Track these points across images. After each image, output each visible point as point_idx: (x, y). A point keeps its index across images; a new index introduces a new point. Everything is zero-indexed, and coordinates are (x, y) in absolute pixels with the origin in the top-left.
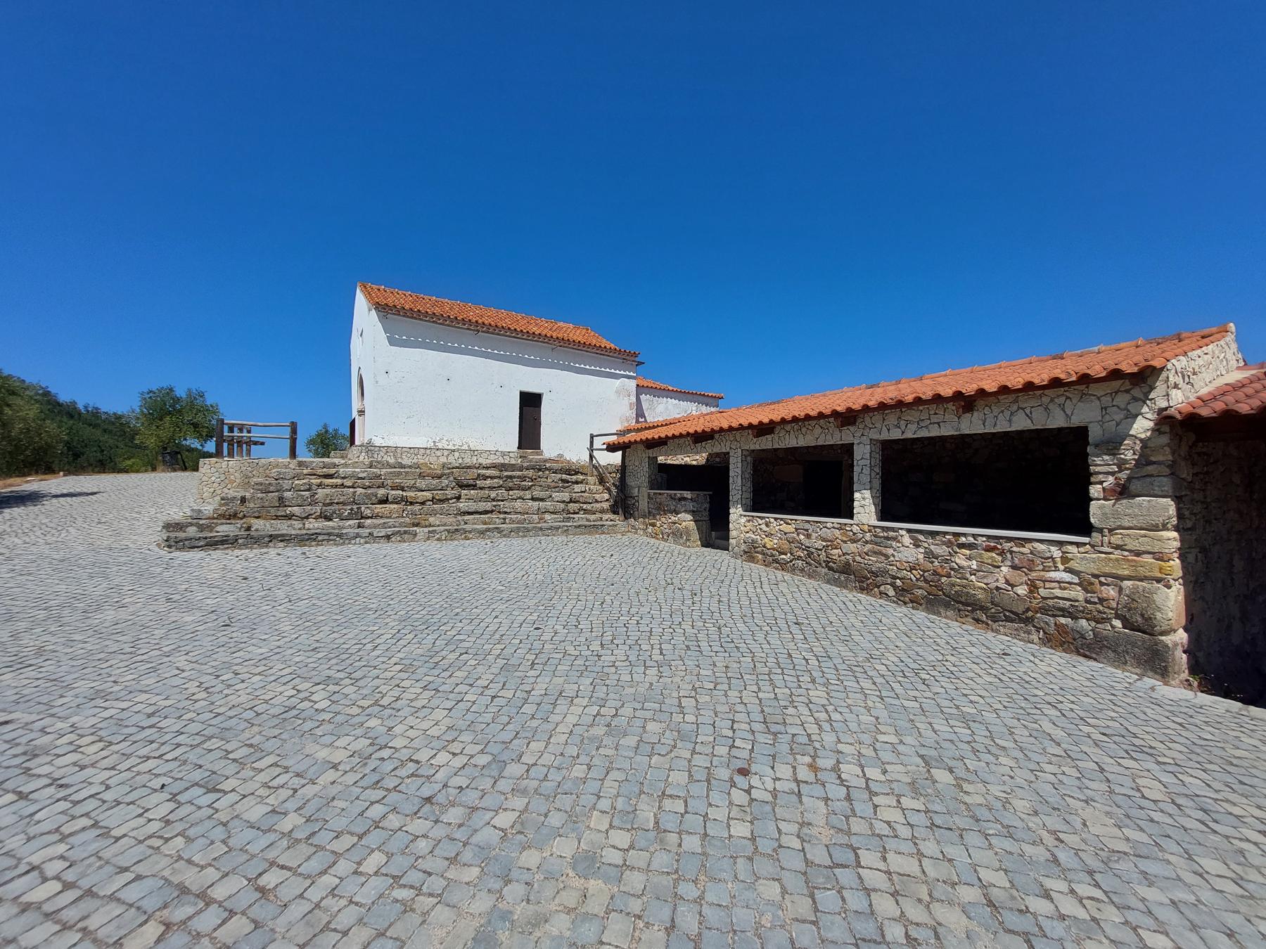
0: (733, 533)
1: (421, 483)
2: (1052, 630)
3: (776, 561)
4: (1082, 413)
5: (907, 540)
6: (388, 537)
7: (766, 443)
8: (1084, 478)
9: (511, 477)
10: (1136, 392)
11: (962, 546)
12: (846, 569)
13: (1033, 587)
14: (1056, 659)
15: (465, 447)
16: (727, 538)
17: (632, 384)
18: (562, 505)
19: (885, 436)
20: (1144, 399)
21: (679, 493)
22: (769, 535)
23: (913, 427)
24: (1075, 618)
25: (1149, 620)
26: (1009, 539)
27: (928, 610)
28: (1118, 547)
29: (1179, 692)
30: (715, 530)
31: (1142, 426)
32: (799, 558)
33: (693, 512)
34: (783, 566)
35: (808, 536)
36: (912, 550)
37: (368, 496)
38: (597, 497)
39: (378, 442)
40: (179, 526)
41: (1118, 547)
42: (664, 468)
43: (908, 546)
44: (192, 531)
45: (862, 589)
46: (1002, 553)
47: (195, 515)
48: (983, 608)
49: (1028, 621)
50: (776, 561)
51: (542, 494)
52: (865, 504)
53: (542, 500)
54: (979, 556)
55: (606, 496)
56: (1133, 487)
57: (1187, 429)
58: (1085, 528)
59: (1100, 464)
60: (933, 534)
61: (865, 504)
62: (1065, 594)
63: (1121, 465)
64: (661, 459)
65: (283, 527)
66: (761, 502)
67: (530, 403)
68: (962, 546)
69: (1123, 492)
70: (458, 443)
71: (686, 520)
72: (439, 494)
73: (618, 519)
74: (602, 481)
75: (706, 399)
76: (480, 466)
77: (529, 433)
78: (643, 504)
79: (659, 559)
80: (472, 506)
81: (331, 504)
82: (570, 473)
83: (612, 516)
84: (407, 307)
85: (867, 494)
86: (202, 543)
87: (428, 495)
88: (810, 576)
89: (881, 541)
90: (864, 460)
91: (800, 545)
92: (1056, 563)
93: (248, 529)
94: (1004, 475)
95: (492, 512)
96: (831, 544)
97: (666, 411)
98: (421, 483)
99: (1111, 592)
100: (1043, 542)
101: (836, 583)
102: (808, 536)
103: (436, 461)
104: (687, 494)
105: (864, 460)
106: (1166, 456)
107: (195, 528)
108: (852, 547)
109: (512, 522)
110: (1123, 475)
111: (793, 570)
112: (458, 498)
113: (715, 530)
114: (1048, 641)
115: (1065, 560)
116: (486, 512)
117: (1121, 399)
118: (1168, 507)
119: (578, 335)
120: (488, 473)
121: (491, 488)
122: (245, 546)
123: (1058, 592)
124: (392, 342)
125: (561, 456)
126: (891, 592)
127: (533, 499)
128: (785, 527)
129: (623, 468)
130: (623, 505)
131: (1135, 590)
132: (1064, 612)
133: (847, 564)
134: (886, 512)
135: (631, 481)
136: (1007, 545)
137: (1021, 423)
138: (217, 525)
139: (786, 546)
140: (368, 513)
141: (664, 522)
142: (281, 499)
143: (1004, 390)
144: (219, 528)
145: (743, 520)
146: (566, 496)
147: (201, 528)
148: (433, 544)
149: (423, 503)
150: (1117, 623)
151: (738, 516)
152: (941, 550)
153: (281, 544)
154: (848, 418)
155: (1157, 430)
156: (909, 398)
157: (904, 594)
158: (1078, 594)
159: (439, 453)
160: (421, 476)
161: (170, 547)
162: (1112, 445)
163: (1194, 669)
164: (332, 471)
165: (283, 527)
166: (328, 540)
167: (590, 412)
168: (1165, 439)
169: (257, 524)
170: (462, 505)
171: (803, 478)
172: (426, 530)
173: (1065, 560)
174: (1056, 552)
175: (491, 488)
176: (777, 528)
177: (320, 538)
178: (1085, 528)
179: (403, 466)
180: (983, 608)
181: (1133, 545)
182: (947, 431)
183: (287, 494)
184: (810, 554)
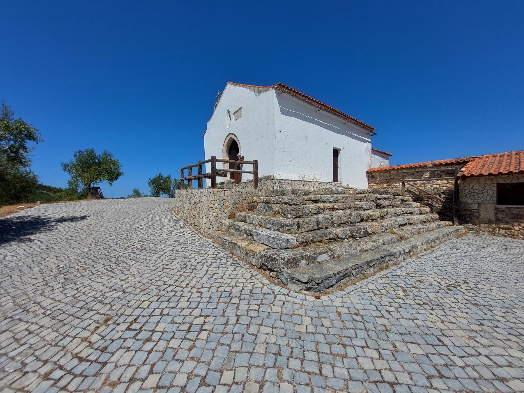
17: (370, 146)
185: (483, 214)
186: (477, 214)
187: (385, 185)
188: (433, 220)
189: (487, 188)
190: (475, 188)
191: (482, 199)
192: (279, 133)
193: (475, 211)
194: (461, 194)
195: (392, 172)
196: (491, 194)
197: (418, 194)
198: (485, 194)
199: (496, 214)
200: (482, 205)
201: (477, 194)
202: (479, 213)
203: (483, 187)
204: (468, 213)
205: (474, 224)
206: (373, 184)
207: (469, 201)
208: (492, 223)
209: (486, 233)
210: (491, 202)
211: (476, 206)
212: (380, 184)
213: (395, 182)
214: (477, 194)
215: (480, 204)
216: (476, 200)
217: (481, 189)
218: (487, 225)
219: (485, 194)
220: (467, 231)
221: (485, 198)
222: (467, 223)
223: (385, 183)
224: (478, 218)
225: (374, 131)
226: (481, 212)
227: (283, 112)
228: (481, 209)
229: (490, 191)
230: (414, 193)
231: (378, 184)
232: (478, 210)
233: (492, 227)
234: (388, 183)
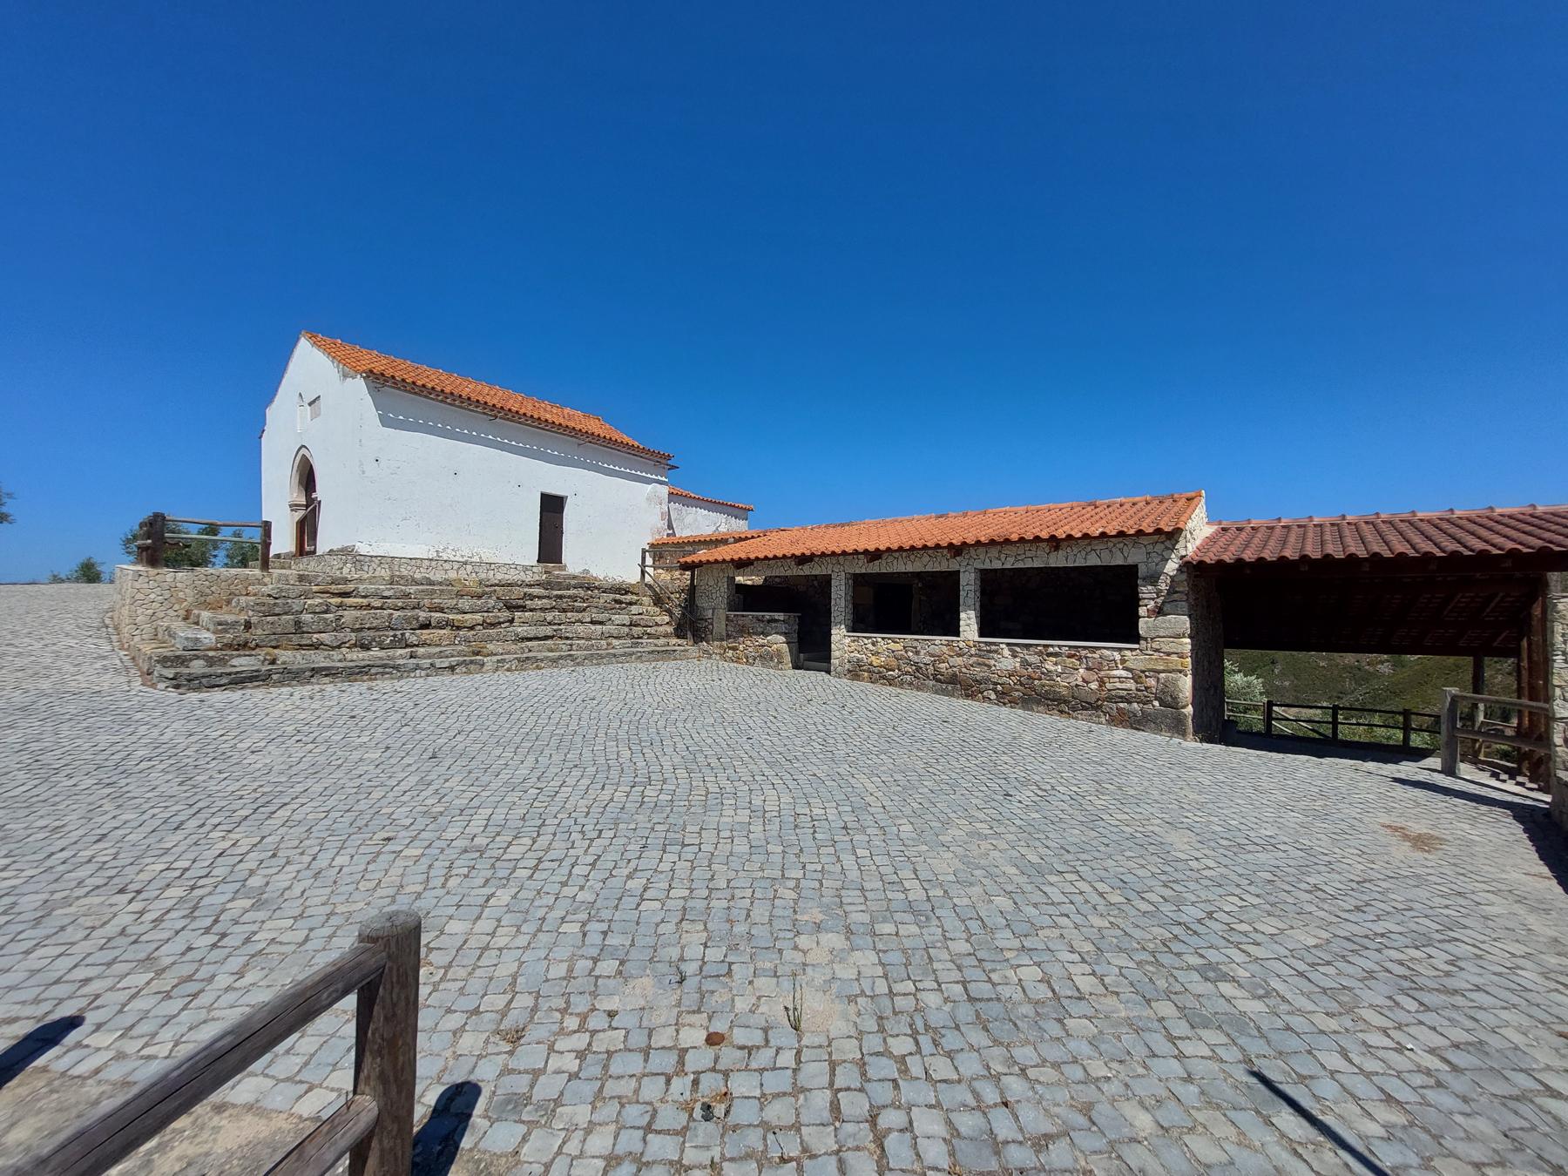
0: (835, 653)
1: (465, 603)
2: (1114, 712)
3: (884, 678)
4: (1134, 556)
5: (1006, 652)
6: (452, 668)
7: (875, 568)
8: (1135, 601)
9: (561, 597)
10: (1168, 544)
11: (1050, 655)
12: (953, 680)
13: (1102, 682)
14: (1120, 733)
15: (476, 559)
16: (828, 659)
17: (664, 491)
18: (626, 629)
19: (987, 566)
20: (1173, 549)
21: (767, 615)
22: (876, 654)
23: (1012, 560)
24: (1129, 703)
25: (1175, 699)
26: (1085, 648)
27: (1024, 708)
28: (1157, 650)
29: (1192, 744)
30: (811, 649)
31: (1171, 567)
32: (907, 673)
33: (784, 634)
34: (891, 682)
35: (917, 653)
36: (1011, 660)
37: (407, 620)
38: (658, 619)
39: (363, 549)
40: (180, 661)
41: (1157, 650)
42: (741, 588)
43: (1007, 657)
44: (197, 667)
45: (967, 696)
46: (1080, 659)
47: (190, 645)
48: (1065, 702)
49: (1098, 708)
50: (884, 678)
51: (601, 617)
52: (969, 622)
53: (601, 623)
54: (1064, 662)
55: (667, 619)
56: (1167, 608)
57: (1194, 569)
58: (1132, 636)
59: (1146, 591)
60: (1027, 646)
61: (969, 622)
62: (1123, 686)
63: (1158, 593)
64: (739, 579)
65: (319, 659)
66: (859, 624)
67: (552, 507)
68: (1050, 655)
69: (1160, 611)
70: (467, 553)
71: (778, 642)
72: (490, 617)
73: (685, 644)
74: (658, 601)
75: (736, 512)
76: (523, 584)
77: (550, 546)
78: (720, 626)
79: (748, 685)
80: (532, 631)
81: (361, 630)
82: (620, 593)
83: (680, 641)
84: (447, 390)
85: (972, 614)
86: (224, 681)
87: (478, 617)
88: (918, 689)
89: (984, 654)
90: (969, 585)
91: (909, 661)
92: (1117, 664)
93: (273, 662)
94: (1065, 598)
95: (552, 637)
96: (939, 658)
97: (699, 523)
98: (465, 603)
99: (1152, 682)
100: (1108, 650)
101: (944, 692)
102: (917, 653)
103: (469, 577)
104: (780, 616)
105: (969, 585)
106: (1184, 588)
107: (202, 662)
108: (959, 661)
109: (580, 648)
110: (1160, 600)
111: (901, 685)
112: (512, 621)
113: (811, 649)
114: (1113, 721)
115: (1123, 661)
116: (546, 638)
117: (1159, 547)
118: (1183, 622)
119: (593, 426)
120: (536, 591)
121: (543, 610)
122: (280, 683)
123: (1118, 685)
124: (385, 422)
125: (586, 571)
126: (993, 696)
127: (592, 622)
128: (892, 646)
129: (692, 590)
130: (691, 626)
131: (1167, 680)
132: (1123, 699)
133: (955, 675)
134: (987, 628)
135: (701, 602)
136: (1083, 653)
137: (1093, 561)
138: (232, 657)
139: (894, 663)
140: (413, 639)
141: (748, 645)
142: (298, 623)
143: (1086, 536)
144: (235, 662)
145: (847, 640)
146: (626, 619)
147: (211, 662)
148: (502, 676)
149: (472, 628)
150: (1156, 703)
151: (841, 639)
152: (1033, 659)
153: (327, 680)
154: (956, 550)
155: (1179, 570)
156: (1015, 537)
157: (1004, 697)
158: (1131, 685)
159: (447, 566)
160: (460, 595)
161: (177, 687)
162: (1153, 579)
163: (1196, 733)
164: (350, 587)
165: (319, 659)
166: (383, 674)
167: (620, 526)
168: (1184, 576)
169: (285, 656)
170: (522, 631)
171: (903, 598)
172: (495, 658)
173: (1123, 661)
174: (1117, 656)
175: (543, 610)
176: (884, 647)
177: (373, 671)
178: (1132, 636)
179: (431, 583)
180: (1065, 702)
181: (1166, 648)
182: (1037, 564)
183: (306, 617)
184: (918, 669)
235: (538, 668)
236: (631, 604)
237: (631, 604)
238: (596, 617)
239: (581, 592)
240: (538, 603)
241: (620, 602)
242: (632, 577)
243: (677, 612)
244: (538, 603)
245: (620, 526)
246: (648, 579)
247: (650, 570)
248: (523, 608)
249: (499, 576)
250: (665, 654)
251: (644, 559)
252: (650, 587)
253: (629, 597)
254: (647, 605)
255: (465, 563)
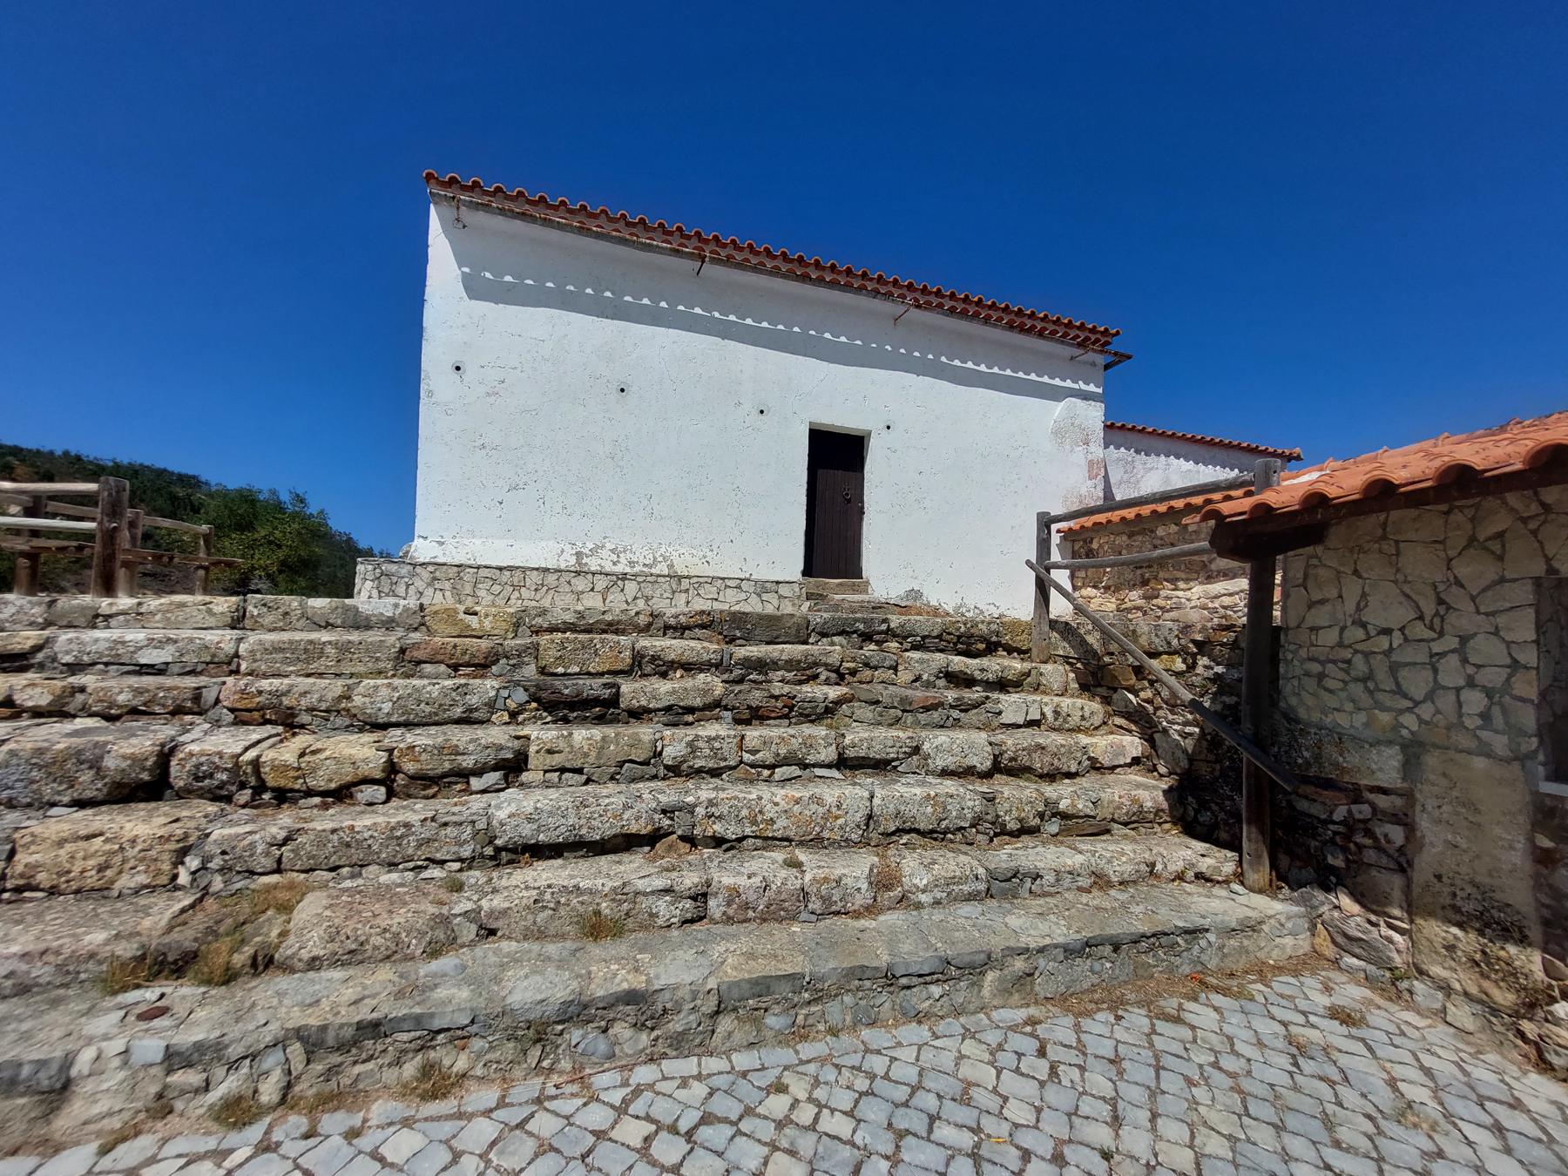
17: (1094, 415)
37: (55, 767)
55: (1133, 745)
67: (836, 457)
70: (642, 555)
73: (1224, 896)
74: (1096, 677)
77: (832, 540)
121: (678, 714)
127: (845, 763)
149: (341, 794)
159: (581, 584)
185: (1437, 841)
186: (1397, 834)
187: (1134, 597)
188: (1137, 820)
189: (1464, 619)
190: (1375, 618)
191: (1426, 711)
192: (455, 376)
193: (1382, 801)
194: (1293, 665)
195: (1160, 532)
196: (1493, 677)
197: (1096, 646)
198: (1451, 672)
199: (1544, 859)
200: (1432, 760)
201: (1394, 669)
202: (1410, 828)
203: (1429, 608)
204: (1340, 813)
205: (1369, 900)
206: (1089, 591)
207: (1342, 720)
208: (1511, 932)
209: (1462, 1014)
210: (1500, 743)
211: (1385, 767)
212: (1117, 589)
213: (1173, 581)
214: (1394, 669)
215: (1413, 752)
216: (1385, 718)
217: (1420, 631)
218: (1468, 941)
219: (1451, 672)
220: (1330, 951)
221: (1446, 702)
222: (1327, 889)
223: (1133, 587)
224: (1403, 867)
225: (1116, 345)
226: (1424, 824)
227: (475, 289)
228: (1426, 796)
229: (1486, 649)
230: (1084, 642)
231: (1107, 588)
232: (1408, 795)
233: (1511, 974)
234: (1145, 583)
235: (435, 1084)
236: (1002, 685)
237: (1003, 685)
238: (863, 736)
239: (835, 650)
240: (664, 690)
241: (966, 681)
242: (1008, 598)
243: (1180, 729)
244: (664, 690)
245: (988, 480)
246: (1060, 607)
247: (1061, 577)
248: (605, 709)
249: (699, 605)
250: (1140, 965)
251: (1043, 545)
252: (1065, 630)
253: (995, 665)
254: (1057, 692)
255: (624, 577)
